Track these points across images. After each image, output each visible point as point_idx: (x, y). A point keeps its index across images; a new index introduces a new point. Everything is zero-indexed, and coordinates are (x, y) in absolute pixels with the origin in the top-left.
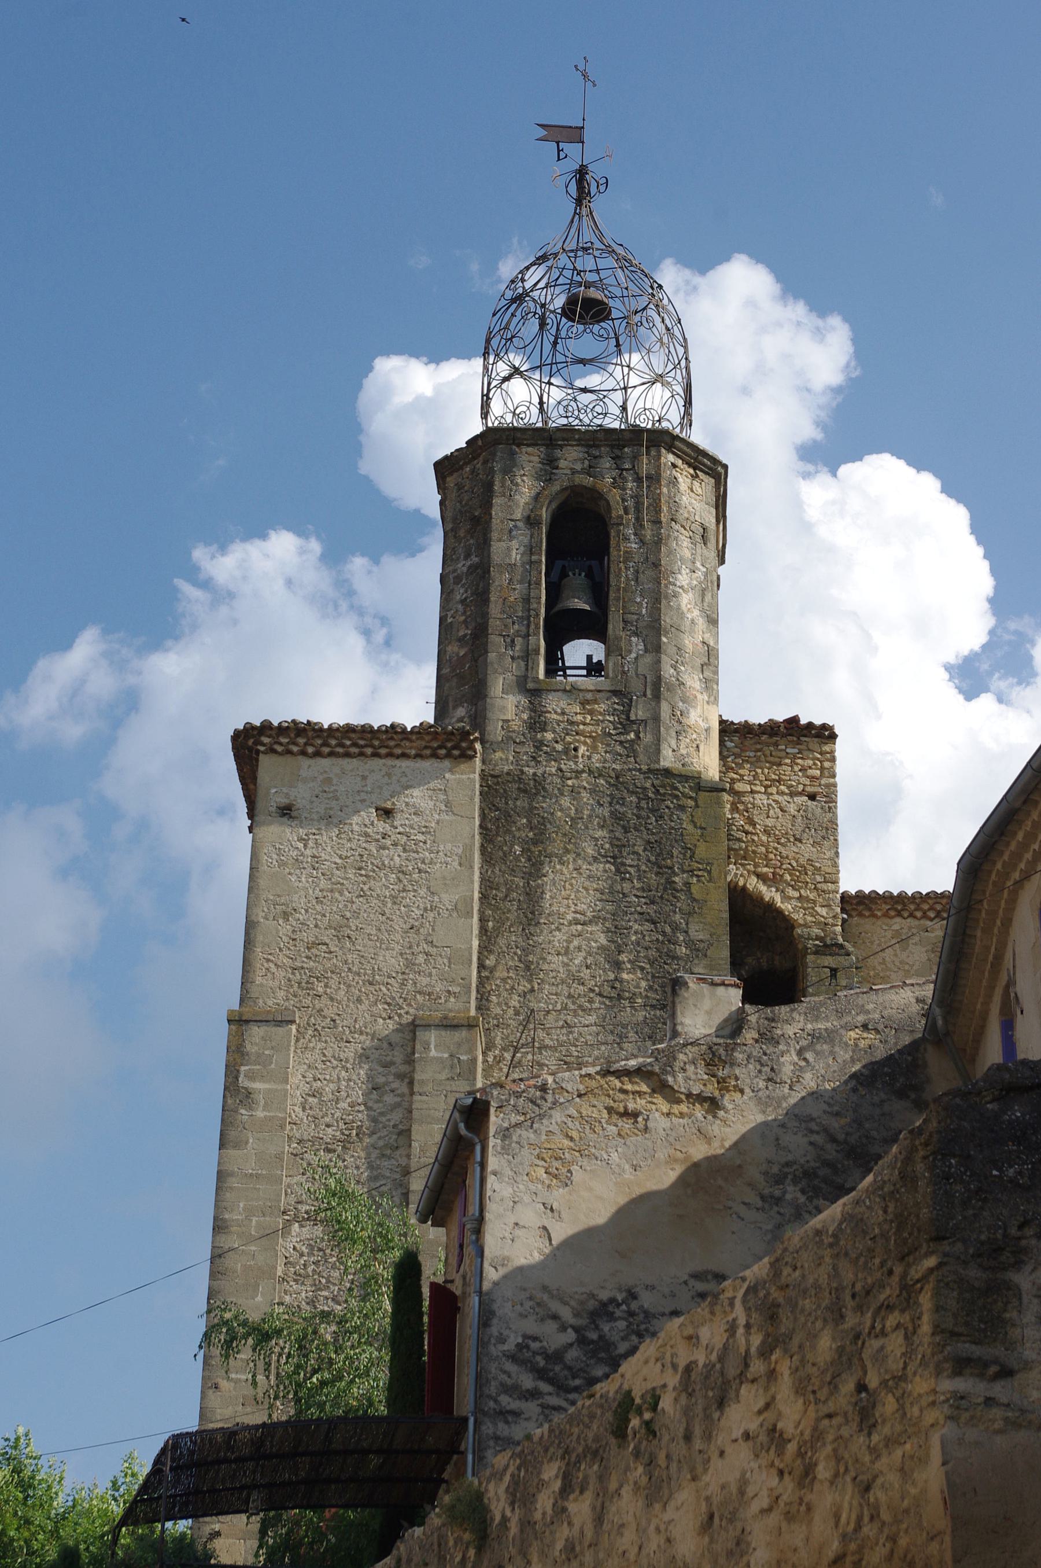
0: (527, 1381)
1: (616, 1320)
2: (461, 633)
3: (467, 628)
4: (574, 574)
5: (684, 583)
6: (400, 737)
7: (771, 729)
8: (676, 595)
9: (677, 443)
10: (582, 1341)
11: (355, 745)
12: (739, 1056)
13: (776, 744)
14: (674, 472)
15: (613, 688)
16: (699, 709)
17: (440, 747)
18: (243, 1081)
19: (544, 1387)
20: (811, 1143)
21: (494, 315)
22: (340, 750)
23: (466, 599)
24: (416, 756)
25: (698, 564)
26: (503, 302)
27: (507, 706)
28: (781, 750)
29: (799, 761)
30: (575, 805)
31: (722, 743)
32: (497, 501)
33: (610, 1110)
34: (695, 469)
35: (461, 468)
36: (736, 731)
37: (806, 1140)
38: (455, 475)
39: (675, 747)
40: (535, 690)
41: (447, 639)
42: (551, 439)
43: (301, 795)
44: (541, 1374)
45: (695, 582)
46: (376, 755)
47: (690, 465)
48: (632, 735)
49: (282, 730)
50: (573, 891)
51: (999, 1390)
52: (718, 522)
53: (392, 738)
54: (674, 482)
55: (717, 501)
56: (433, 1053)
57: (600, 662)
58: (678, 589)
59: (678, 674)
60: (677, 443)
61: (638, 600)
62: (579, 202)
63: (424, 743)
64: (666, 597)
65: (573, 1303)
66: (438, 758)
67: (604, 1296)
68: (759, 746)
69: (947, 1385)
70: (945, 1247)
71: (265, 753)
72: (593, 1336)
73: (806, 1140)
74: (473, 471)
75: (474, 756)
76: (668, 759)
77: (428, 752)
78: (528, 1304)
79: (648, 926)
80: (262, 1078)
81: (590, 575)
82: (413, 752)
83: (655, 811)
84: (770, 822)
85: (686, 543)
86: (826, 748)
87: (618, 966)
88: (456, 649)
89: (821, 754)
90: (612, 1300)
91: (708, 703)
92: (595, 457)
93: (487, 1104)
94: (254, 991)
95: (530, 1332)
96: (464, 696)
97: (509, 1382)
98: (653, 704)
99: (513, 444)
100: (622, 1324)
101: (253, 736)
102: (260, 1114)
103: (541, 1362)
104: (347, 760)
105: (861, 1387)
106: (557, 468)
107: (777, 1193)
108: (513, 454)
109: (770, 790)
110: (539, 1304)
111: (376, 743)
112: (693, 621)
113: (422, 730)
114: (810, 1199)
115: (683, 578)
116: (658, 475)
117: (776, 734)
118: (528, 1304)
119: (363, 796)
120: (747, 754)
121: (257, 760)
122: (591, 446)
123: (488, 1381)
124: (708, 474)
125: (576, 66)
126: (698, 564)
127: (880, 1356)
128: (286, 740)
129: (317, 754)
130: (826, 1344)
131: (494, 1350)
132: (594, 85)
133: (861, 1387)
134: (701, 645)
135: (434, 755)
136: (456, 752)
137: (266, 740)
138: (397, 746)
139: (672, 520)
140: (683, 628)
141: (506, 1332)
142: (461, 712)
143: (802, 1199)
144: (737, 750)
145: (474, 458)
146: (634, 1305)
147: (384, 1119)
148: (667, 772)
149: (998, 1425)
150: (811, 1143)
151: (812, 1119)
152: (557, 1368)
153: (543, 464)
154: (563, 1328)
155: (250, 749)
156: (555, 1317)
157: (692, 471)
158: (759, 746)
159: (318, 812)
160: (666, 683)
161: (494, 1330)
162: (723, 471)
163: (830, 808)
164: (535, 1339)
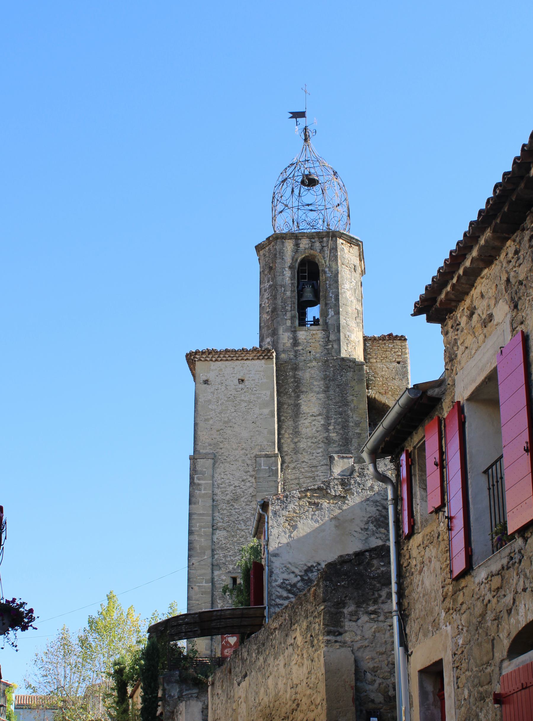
0: (285, 594)
1: (313, 572)
2: (267, 310)
7: (383, 338)
8: (345, 292)
10: (302, 580)
11: (229, 356)
12: (352, 482)
13: (385, 344)
16: (355, 334)
17: (260, 356)
18: (196, 481)
19: (291, 596)
20: (377, 510)
22: (225, 359)
24: (252, 359)
25: (353, 280)
26: (278, 182)
27: (285, 338)
30: (311, 374)
31: (365, 345)
32: (278, 261)
33: (309, 503)
34: (350, 244)
35: (265, 248)
36: (370, 340)
37: (376, 509)
43: (211, 376)
44: (289, 591)
46: (237, 360)
47: (348, 243)
48: (330, 346)
50: (312, 404)
51: (339, 638)
52: (360, 260)
55: (360, 255)
56: (263, 467)
62: (306, 140)
63: (254, 355)
64: (341, 294)
65: (299, 567)
67: (309, 565)
69: (326, 638)
70: (326, 603)
72: (306, 578)
73: (376, 509)
74: (269, 249)
76: (343, 354)
77: (256, 358)
78: (284, 569)
79: (339, 416)
80: (202, 480)
83: (341, 373)
85: (348, 272)
86: (403, 344)
87: (327, 430)
88: (266, 316)
90: (312, 566)
92: (313, 242)
93: (268, 503)
94: (198, 448)
95: (285, 578)
97: (279, 594)
100: (316, 574)
102: (203, 492)
103: (289, 588)
104: (227, 362)
105: (311, 636)
107: (366, 527)
108: (283, 243)
109: (383, 361)
110: (288, 568)
111: (237, 355)
113: (254, 350)
114: (377, 529)
117: (385, 340)
118: (284, 569)
123: (272, 595)
126: (353, 280)
127: (314, 629)
129: (216, 360)
130: (305, 625)
131: (274, 584)
133: (311, 636)
135: (258, 359)
136: (266, 357)
141: (277, 578)
142: (268, 340)
143: (375, 529)
144: (370, 347)
145: (269, 244)
146: (319, 567)
147: (246, 491)
148: (343, 359)
149: (338, 647)
150: (377, 510)
151: (378, 502)
152: (295, 589)
154: (296, 576)
155: (192, 360)
156: (293, 572)
157: (349, 245)
161: (273, 578)
162: (361, 244)
164: (287, 580)
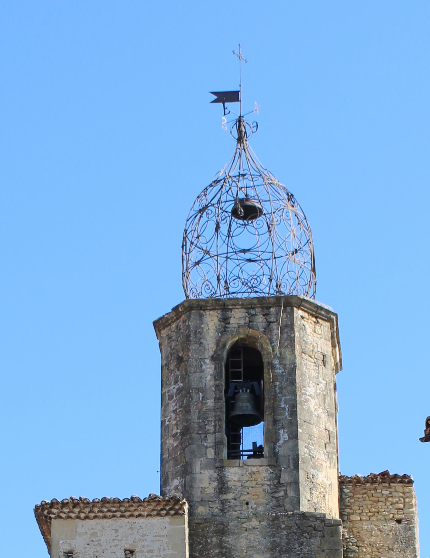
2: (174, 432)
3: (178, 429)
4: (243, 391)
5: (311, 393)
6: (137, 504)
7: (372, 479)
9: (303, 303)
11: (109, 511)
13: (375, 489)
14: (303, 322)
15: (269, 463)
17: (162, 510)
21: (188, 220)
23: (176, 410)
24: (148, 515)
25: (321, 379)
26: (193, 212)
27: (205, 480)
28: (378, 493)
29: (390, 499)
34: (316, 318)
35: (170, 325)
36: (350, 482)
38: (166, 329)
39: (310, 499)
40: (221, 467)
41: (165, 435)
42: (224, 305)
45: (319, 391)
46: (122, 516)
48: (282, 493)
49: (64, 504)
52: (333, 346)
53: (132, 506)
54: (303, 328)
55: (332, 337)
57: (261, 446)
58: (308, 397)
59: (310, 451)
60: (303, 303)
61: (283, 406)
62: (240, 140)
63: (152, 508)
64: (301, 403)
66: (161, 516)
68: (364, 491)
71: (55, 518)
74: (177, 327)
75: (183, 514)
76: (305, 507)
77: (155, 513)
81: (253, 391)
82: (146, 513)
84: (373, 539)
85: (312, 366)
86: (407, 490)
88: (171, 442)
89: (404, 493)
91: (330, 468)
92: (253, 315)
96: (177, 472)
98: (295, 472)
99: (201, 309)
101: (47, 509)
106: (229, 323)
108: (201, 316)
112: (318, 416)
113: (152, 499)
115: (311, 390)
116: (292, 324)
117: (375, 482)
119: (116, 542)
120: (358, 496)
121: (50, 523)
122: (250, 308)
124: (325, 320)
125: (233, 52)
126: (321, 379)
128: (68, 510)
129: (87, 517)
132: (246, 62)
134: (324, 431)
137: (55, 511)
138: (135, 510)
139: (303, 352)
140: (312, 422)
142: (176, 482)
144: (351, 494)
145: (177, 319)
148: (304, 516)
153: (220, 321)
155: (46, 517)
157: (314, 319)
158: (364, 491)
159: (89, 554)
160: (302, 459)
162: (334, 318)
163: (410, 528)
